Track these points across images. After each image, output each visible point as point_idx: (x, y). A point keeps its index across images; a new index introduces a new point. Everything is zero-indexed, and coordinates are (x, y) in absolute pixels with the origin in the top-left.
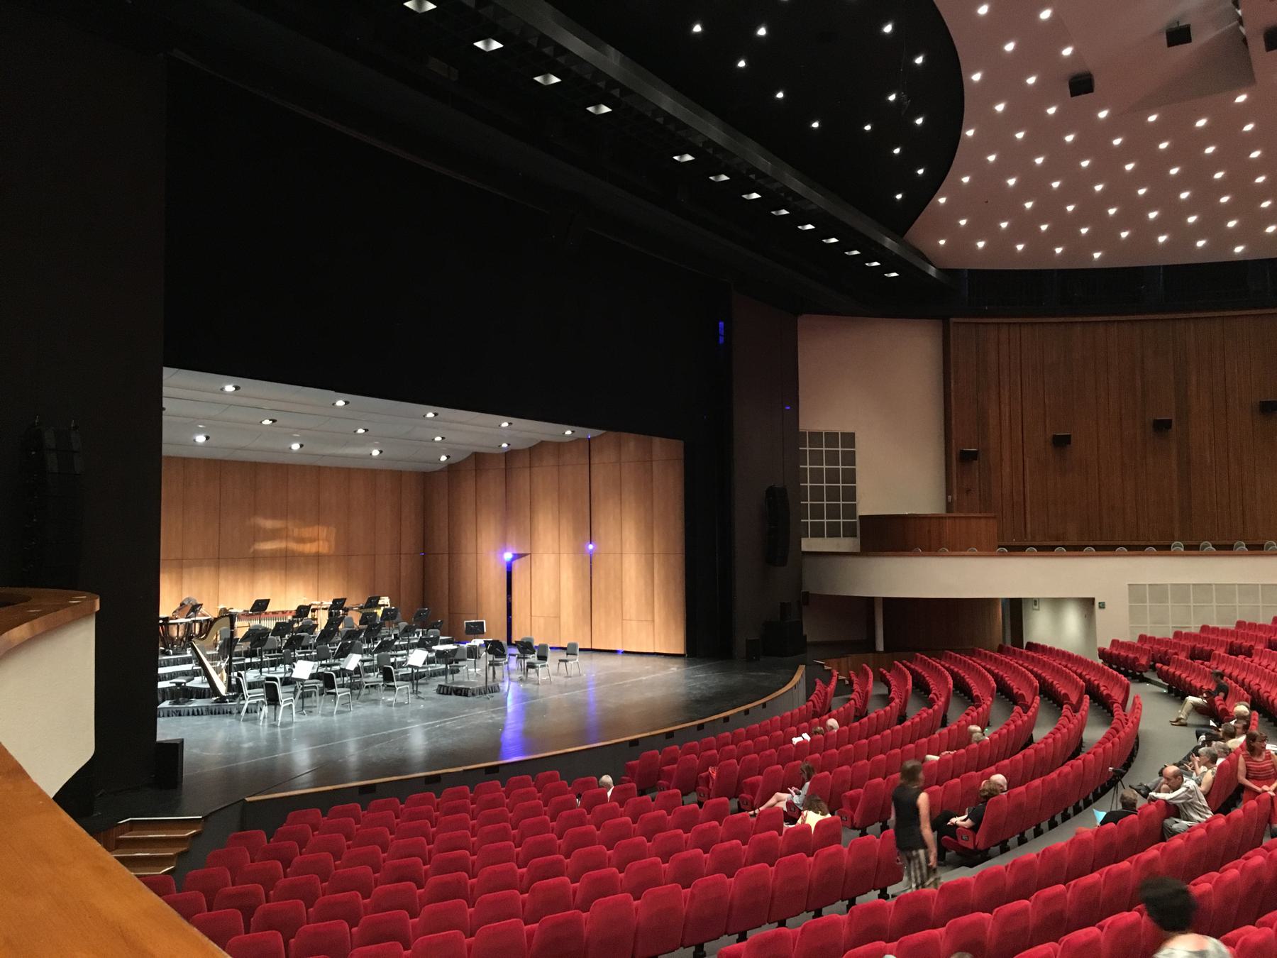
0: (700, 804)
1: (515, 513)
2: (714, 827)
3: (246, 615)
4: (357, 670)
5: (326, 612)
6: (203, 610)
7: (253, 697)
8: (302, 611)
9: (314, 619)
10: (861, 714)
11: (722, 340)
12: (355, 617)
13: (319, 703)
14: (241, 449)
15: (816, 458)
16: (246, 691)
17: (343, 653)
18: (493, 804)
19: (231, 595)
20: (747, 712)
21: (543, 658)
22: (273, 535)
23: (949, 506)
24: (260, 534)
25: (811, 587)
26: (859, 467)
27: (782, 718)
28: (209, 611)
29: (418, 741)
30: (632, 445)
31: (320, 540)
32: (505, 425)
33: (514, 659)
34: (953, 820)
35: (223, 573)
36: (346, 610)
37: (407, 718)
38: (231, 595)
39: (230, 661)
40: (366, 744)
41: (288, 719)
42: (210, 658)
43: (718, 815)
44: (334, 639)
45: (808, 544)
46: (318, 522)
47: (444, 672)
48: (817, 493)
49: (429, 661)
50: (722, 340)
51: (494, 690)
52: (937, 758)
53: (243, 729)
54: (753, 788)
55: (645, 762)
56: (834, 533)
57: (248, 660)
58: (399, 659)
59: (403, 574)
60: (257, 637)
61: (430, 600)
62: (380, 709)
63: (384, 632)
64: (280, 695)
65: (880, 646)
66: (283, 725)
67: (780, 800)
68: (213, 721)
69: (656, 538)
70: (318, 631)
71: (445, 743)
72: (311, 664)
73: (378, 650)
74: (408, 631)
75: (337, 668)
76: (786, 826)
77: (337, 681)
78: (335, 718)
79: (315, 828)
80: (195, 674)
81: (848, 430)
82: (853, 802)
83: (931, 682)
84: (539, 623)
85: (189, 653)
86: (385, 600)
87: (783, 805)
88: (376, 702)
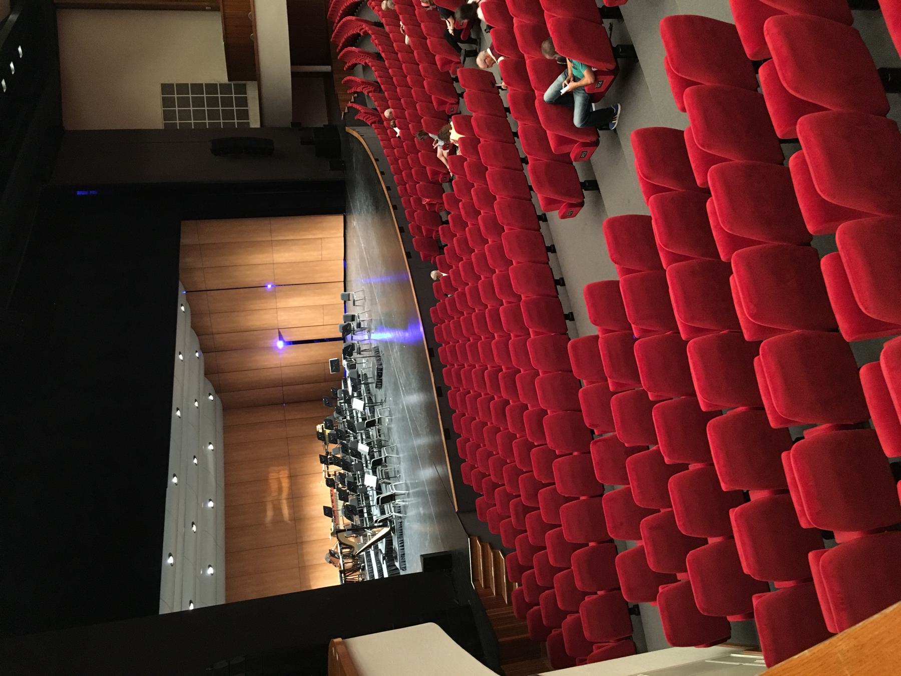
0: (449, 213)
1: (250, 342)
2: (463, 205)
3: (335, 521)
4: (368, 444)
5: (330, 466)
6: (333, 549)
7: (390, 511)
8: (330, 483)
9: (335, 475)
10: (377, 87)
11: (93, 192)
12: (332, 447)
13: (391, 468)
14: (216, 542)
15: (185, 115)
16: (387, 516)
17: (358, 455)
18: (453, 352)
19: (322, 532)
20: (382, 173)
21: (353, 318)
22: (277, 509)
23: (215, 9)
24: (278, 519)
25: (287, 121)
26: (189, 81)
27: (385, 147)
28: (333, 544)
29: (414, 399)
30: (187, 260)
31: (279, 478)
32: (181, 357)
33: (355, 337)
34: (451, 31)
35: (305, 539)
36: (328, 453)
37: (400, 409)
38: (322, 532)
39: (367, 528)
40: (418, 435)
41: (404, 486)
42: (365, 541)
43: (455, 201)
44: (348, 461)
45: (255, 122)
46: (265, 480)
47: (367, 384)
48: (213, 115)
49: (360, 397)
50: (93, 192)
51: (377, 350)
52: (407, 37)
53: (411, 513)
54: (435, 173)
55: (423, 248)
56: (243, 102)
57: (366, 515)
58: (359, 415)
59: (299, 417)
60: (350, 512)
61: (318, 396)
62: (393, 426)
63: (341, 427)
64: (389, 493)
65: (328, 68)
66: (408, 489)
67: (442, 154)
68: (406, 532)
69: (259, 239)
70: (342, 471)
71: (415, 384)
72: (366, 475)
73: (353, 430)
74: (340, 412)
75: (368, 457)
76: (459, 153)
77: (377, 457)
78: (401, 455)
79: (473, 467)
80: (376, 548)
81: (159, 89)
82: (442, 103)
83: (351, 32)
84: (328, 319)
85: (364, 553)
86: (319, 428)
87: (446, 152)
88: (389, 429)
